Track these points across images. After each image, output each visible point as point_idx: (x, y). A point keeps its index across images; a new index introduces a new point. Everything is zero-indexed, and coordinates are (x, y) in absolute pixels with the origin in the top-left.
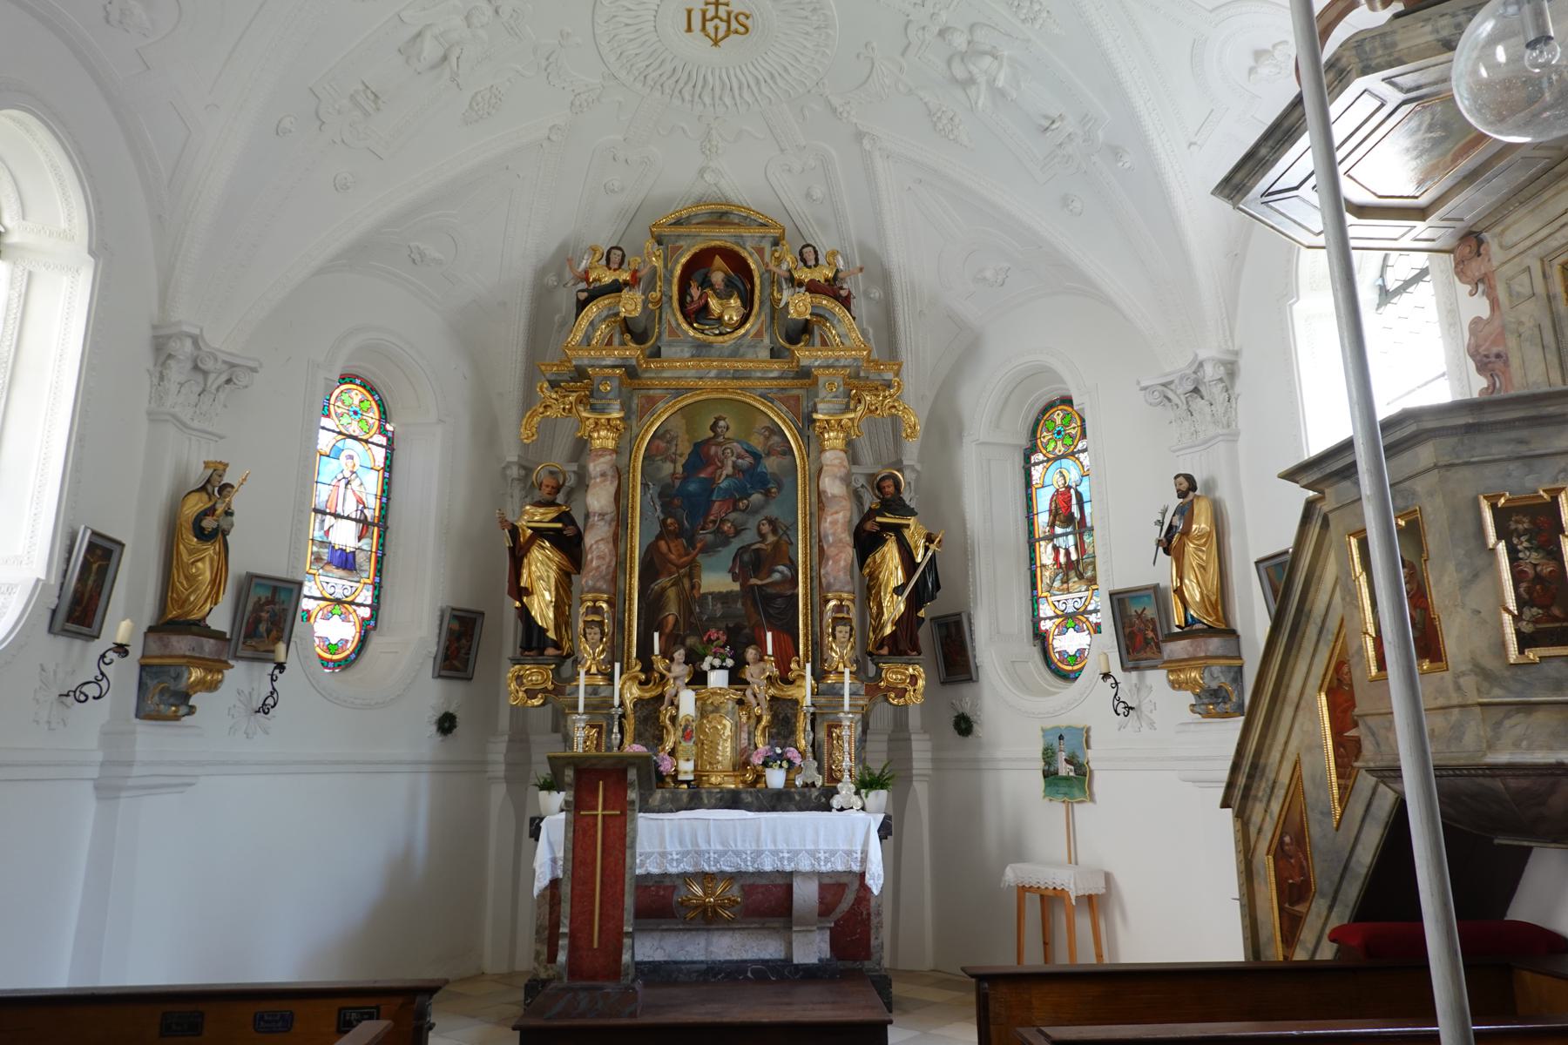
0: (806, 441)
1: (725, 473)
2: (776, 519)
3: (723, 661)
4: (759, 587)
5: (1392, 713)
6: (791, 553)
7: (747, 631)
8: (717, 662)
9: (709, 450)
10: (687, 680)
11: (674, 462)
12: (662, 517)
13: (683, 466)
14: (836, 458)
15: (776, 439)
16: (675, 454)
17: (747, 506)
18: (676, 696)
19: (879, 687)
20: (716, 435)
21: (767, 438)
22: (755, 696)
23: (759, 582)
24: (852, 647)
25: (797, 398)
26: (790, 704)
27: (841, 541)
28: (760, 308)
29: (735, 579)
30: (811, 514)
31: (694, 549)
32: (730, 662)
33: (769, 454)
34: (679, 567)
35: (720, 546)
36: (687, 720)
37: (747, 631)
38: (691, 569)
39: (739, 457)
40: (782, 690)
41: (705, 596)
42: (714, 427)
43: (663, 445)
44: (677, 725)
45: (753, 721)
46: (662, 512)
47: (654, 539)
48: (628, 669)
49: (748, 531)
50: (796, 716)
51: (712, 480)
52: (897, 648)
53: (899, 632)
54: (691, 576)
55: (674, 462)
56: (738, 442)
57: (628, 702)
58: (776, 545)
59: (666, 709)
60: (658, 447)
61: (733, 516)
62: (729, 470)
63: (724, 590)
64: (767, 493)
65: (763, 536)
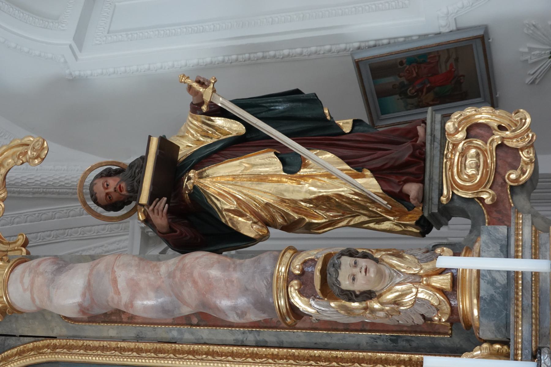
0: (11, 341)
5: (448, 50)
14: (22, 282)
19: (495, 204)
24: (398, 255)
27: (171, 275)
28: (539, 306)
30: (138, 339)
52: (407, 164)
53: (377, 164)
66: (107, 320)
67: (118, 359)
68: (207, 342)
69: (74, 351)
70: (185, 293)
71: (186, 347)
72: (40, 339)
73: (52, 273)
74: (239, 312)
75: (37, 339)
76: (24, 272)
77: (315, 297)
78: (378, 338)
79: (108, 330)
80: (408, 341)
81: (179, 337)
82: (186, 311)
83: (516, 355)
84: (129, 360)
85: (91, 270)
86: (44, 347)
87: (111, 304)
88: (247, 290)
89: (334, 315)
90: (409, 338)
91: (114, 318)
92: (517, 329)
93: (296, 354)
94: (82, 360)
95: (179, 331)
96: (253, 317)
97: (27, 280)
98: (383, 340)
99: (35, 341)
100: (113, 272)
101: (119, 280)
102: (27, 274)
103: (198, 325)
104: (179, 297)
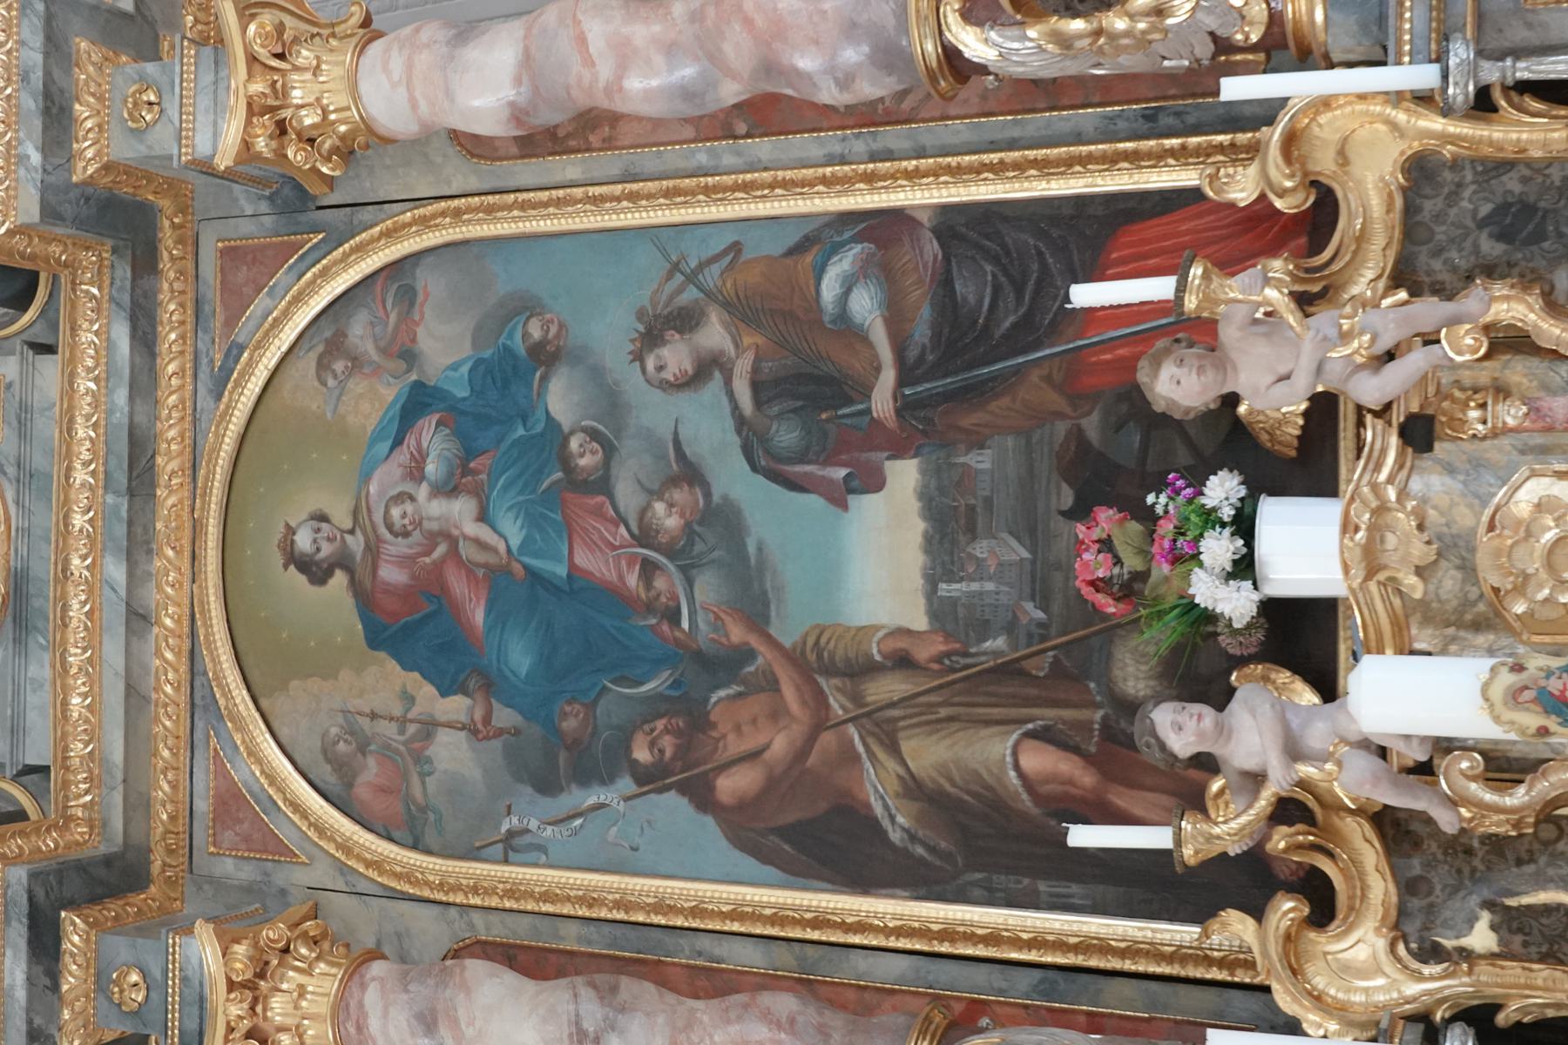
0: (366, 214)
1: (472, 528)
2: (641, 315)
3: (1210, 518)
4: (903, 380)
6: (774, 246)
7: (1092, 425)
8: (1219, 548)
9: (390, 590)
10: (1307, 696)
11: (430, 727)
12: (626, 784)
13: (444, 693)
14: (386, 69)
15: (359, 331)
16: (403, 722)
17: (594, 435)
18: (1383, 752)
20: (343, 561)
21: (357, 363)
22: (1390, 356)
23: (888, 377)
25: (232, 255)
26: (1429, 207)
29: (873, 483)
31: (749, 654)
32: (1223, 490)
33: (409, 356)
34: (821, 723)
35: (742, 547)
36: (1514, 696)
37: (1092, 425)
38: (830, 671)
39: (416, 473)
40: (1362, 238)
41: (940, 611)
42: (316, 571)
43: (371, 771)
44: (1538, 750)
45: (1517, 371)
46: (607, 780)
47: (709, 821)
48: (1250, 965)
49: (684, 434)
50: (1496, 166)
51: (496, 578)
54: (859, 670)
55: (430, 727)
56: (366, 478)
57: (1413, 989)
58: (742, 311)
59: (1453, 803)
60: (382, 790)
61: (627, 495)
62: (460, 512)
63: (917, 527)
64: (545, 356)
65: (707, 367)
66: (559, 150)
67: (592, 218)
68: (769, 165)
69: (499, 214)
70: (728, 49)
71: (728, 180)
72: (425, 202)
73: (448, 43)
74: (840, 75)
75: (417, 203)
76: (387, 50)
77: (995, 22)
78: (1119, 116)
79: (564, 169)
80: (1178, 114)
81: (712, 163)
82: (730, 92)
83: (1399, 54)
84: (614, 217)
85: (529, 29)
86: (434, 216)
87: (575, 93)
88: (854, 25)
89: (1034, 58)
90: (1181, 108)
91: (572, 143)
92: (1401, 15)
93: (954, 164)
94: (518, 231)
95: (709, 151)
96: (870, 88)
97: (397, 63)
98: (1128, 119)
99: (416, 208)
100: (577, 22)
101: (590, 37)
102: (395, 53)
103: (748, 136)
104: (714, 58)
